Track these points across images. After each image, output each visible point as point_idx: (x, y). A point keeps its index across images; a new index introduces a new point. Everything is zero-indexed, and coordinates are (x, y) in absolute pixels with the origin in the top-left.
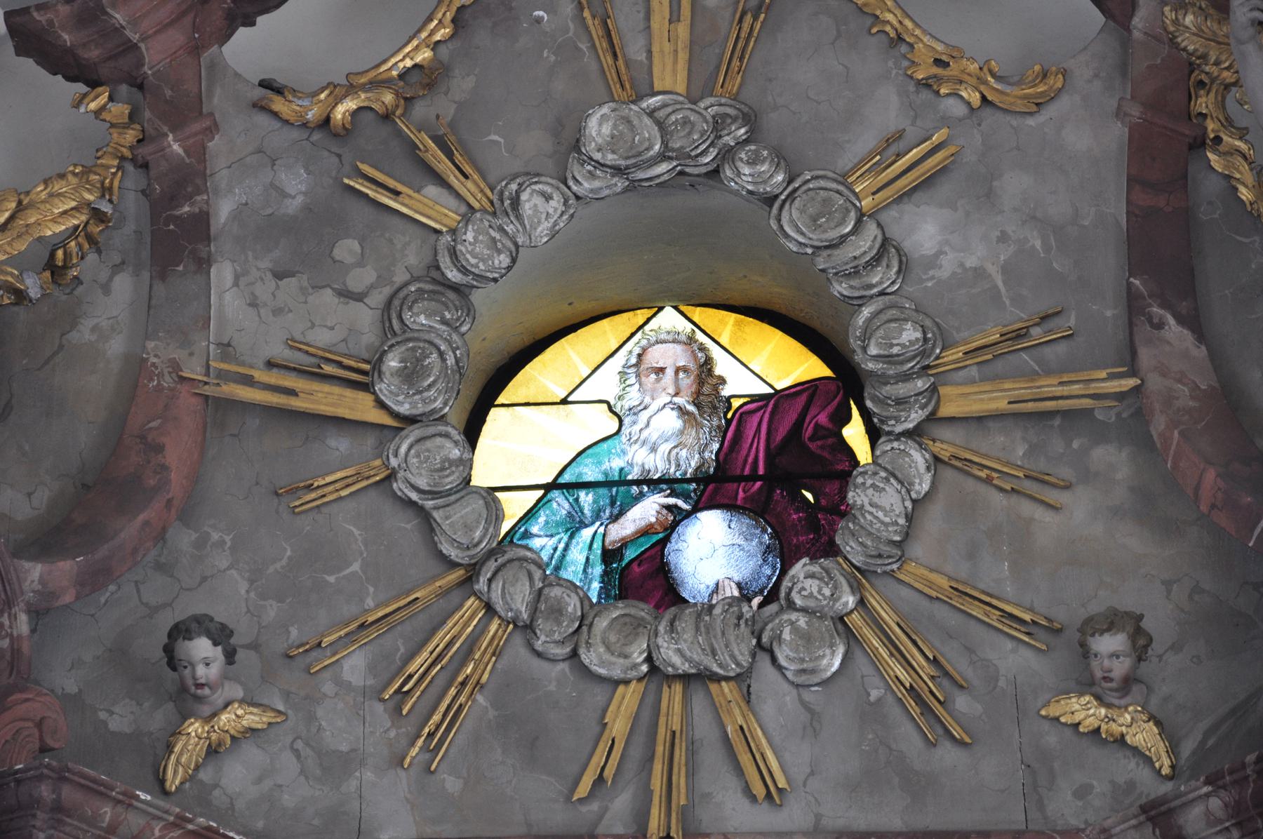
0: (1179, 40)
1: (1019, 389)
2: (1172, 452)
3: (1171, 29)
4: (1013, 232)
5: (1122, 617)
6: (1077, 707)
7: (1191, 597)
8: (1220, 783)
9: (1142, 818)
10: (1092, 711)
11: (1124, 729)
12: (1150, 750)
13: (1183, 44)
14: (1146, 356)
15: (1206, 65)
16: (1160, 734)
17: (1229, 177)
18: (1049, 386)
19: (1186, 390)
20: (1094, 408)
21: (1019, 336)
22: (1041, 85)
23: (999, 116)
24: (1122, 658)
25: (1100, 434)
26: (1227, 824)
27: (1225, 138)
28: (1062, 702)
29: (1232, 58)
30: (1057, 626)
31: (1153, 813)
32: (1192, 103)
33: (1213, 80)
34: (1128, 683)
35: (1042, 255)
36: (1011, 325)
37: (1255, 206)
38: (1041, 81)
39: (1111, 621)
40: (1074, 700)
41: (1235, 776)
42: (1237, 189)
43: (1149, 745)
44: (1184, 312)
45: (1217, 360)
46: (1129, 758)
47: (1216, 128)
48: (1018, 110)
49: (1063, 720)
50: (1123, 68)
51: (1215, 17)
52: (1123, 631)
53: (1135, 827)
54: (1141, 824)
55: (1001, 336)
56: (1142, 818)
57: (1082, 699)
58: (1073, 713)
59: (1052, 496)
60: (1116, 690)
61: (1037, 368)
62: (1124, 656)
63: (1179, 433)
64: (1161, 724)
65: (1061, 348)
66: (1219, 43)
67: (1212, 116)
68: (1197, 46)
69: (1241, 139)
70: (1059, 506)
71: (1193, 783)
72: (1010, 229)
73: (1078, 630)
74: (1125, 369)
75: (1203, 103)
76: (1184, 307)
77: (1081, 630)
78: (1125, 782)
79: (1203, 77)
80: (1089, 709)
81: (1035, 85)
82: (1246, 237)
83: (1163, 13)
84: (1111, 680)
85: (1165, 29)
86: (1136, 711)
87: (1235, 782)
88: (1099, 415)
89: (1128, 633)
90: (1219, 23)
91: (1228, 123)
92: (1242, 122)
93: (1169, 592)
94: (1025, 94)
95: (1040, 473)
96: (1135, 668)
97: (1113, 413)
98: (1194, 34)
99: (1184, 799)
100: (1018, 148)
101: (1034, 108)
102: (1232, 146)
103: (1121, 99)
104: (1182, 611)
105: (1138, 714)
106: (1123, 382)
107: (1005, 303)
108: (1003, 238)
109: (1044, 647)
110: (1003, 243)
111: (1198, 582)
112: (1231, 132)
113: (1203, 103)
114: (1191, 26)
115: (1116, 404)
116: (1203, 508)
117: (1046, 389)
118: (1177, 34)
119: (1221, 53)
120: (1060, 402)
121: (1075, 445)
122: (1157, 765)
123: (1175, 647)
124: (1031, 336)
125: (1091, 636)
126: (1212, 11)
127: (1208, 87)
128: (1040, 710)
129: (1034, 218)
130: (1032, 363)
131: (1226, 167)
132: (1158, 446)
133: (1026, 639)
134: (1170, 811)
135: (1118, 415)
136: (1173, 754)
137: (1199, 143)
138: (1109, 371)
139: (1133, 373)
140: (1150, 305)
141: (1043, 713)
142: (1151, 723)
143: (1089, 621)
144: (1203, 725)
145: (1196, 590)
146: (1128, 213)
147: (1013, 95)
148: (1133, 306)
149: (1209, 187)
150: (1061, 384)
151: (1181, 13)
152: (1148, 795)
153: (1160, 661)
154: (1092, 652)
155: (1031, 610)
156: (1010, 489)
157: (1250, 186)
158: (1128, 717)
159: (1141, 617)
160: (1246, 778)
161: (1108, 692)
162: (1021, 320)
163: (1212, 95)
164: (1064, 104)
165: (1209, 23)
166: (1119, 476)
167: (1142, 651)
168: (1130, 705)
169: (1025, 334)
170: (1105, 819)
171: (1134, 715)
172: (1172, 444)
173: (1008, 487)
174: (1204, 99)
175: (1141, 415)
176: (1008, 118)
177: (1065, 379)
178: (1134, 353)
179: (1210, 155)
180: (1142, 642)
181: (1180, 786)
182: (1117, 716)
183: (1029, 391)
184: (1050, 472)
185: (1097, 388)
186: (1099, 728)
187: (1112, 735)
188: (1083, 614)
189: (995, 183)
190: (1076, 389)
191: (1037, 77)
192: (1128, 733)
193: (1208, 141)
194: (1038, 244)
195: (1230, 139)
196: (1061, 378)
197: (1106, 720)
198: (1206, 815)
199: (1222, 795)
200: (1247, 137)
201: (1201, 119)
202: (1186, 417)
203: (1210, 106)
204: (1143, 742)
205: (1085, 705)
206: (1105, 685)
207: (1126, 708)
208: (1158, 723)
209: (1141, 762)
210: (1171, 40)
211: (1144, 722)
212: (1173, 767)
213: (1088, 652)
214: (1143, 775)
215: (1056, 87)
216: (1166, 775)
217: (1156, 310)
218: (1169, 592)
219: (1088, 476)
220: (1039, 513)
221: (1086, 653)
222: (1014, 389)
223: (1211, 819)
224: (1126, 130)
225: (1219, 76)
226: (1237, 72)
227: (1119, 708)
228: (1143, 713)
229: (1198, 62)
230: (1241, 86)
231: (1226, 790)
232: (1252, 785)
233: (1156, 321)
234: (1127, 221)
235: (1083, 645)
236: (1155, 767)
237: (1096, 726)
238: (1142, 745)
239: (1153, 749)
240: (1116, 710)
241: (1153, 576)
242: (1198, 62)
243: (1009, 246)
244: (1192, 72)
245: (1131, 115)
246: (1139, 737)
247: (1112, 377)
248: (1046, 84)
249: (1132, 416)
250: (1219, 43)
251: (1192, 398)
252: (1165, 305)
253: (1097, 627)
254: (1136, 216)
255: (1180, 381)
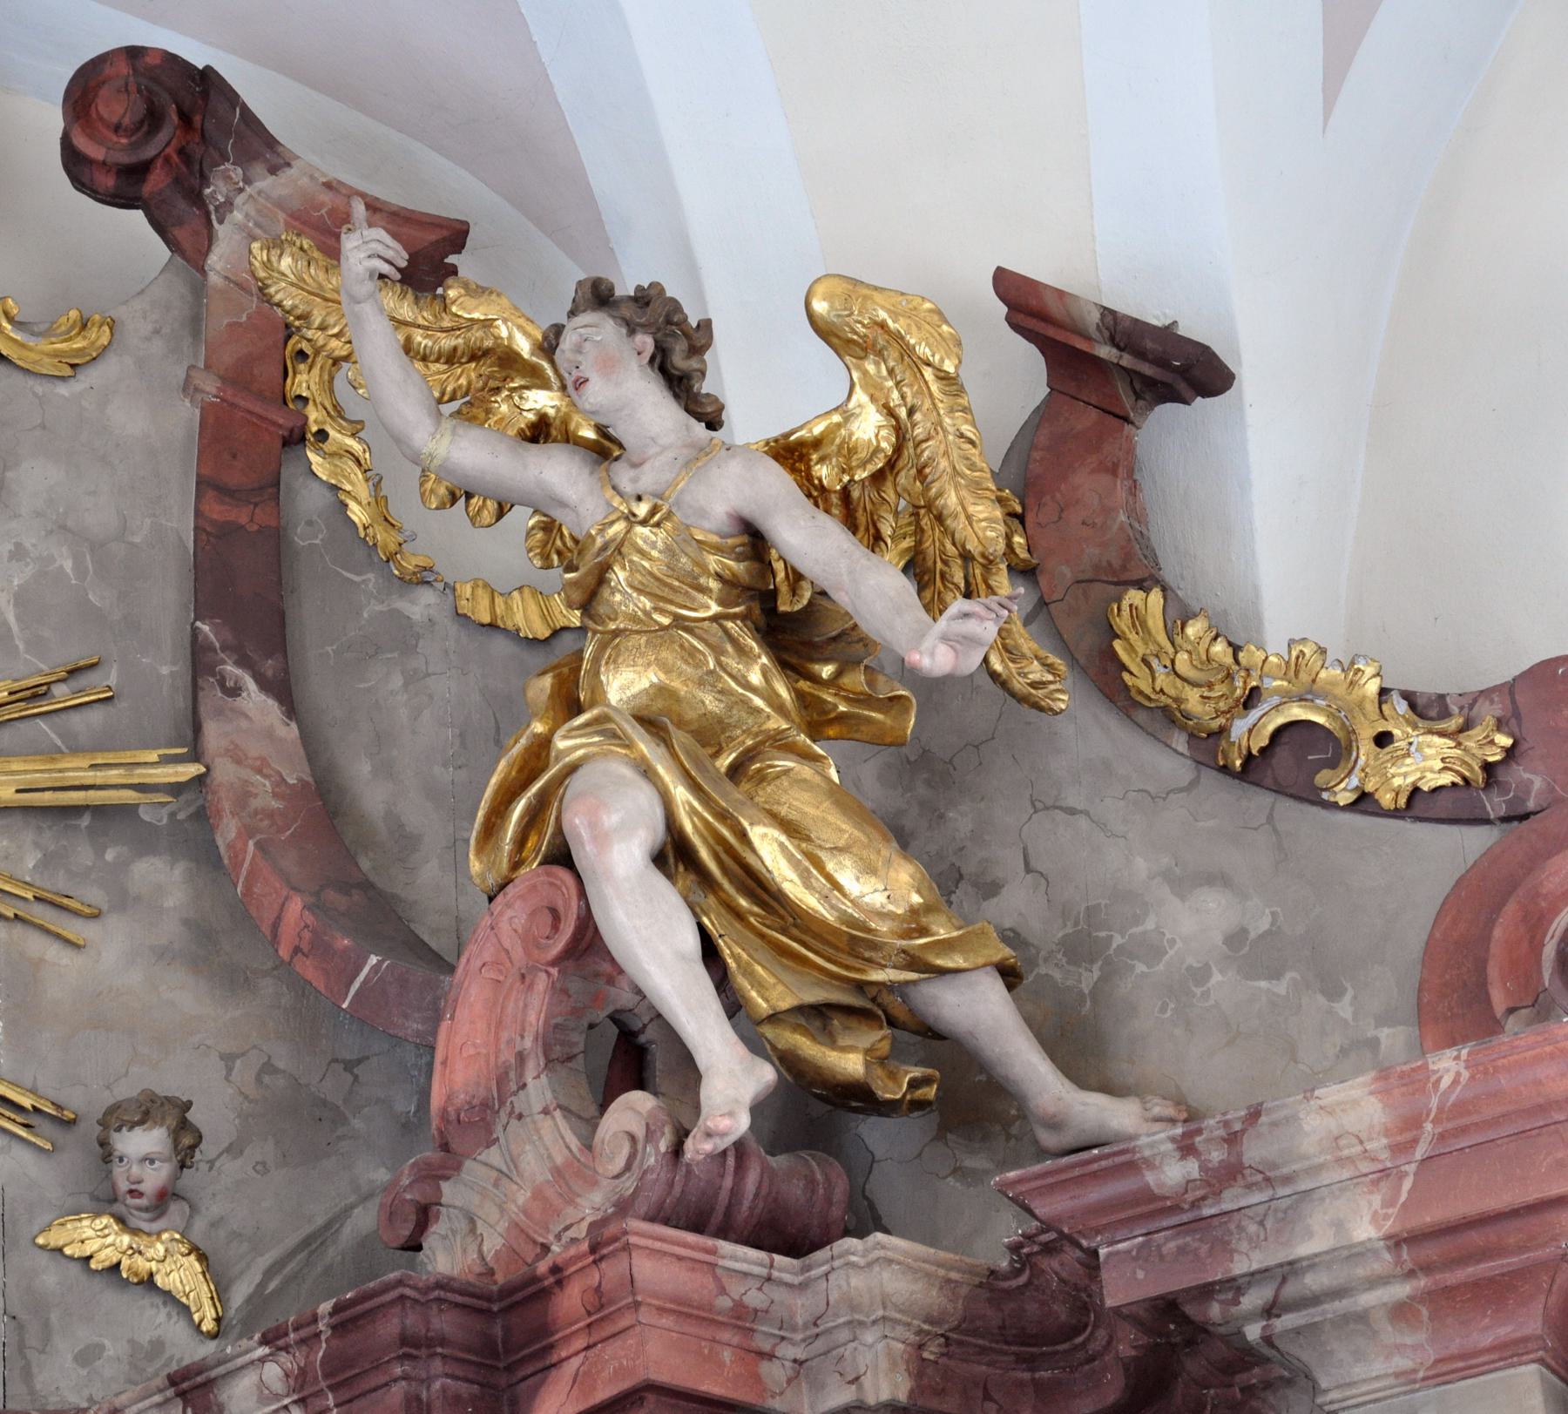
0: (272, 290)
1: (32, 771)
2: (244, 872)
3: (262, 274)
4: (34, 545)
5: (162, 1104)
6: (90, 1233)
7: (259, 1080)
8: (281, 1343)
9: (170, 1392)
10: (110, 1240)
11: (154, 1265)
12: (187, 1296)
13: (278, 298)
14: (214, 734)
15: (309, 328)
16: (203, 1273)
17: (335, 488)
18: (76, 769)
19: (267, 783)
20: (138, 805)
21: (35, 697)
22: (80, 338)
23: (18, 378)
24: (157, 1164)
25: (146, 841)
26: (286, 1401)
27: (332, 433)
28: (69, 1226)
29: (344, 321)
30: (69, 1115)
31: (185, 1385)
32: (289, 381)
33: (317, 352)
34: (164, 1199)
35: (74, 582)
36: (24, 678)
37: (370, 531)
38: (79, 333)
39: (146, 1110)
40: (86, 1223)
41: (303, 1333)
42: (347, 505)
43: (187, 1289)
44: (270, 673)
45: (311, 743)
46: (157, 1307)
47: (320, 418)
48: (45, 372)
49: (68, 1251)
50: (195, 323)
51: (321, 263)
52: (161, 1125)
53: (159, 1405)
54: (167, 1401)
55: (10, 694)
56: (170, 1392)
57: (98, 1221)
58: (83, 1242)
59: (73, 928)
60: (147, 1210)
61: (59, 743)
62: (162, 1161)
63: (257, 844)
64: (207, 1259)
65: (96, 716)
66: (326, 300)
67: (314, 401)
68: (297, 302)
69: (353, 435)
70: (81, 942)
71: (244, 1343)
72: (28, 543)
73: (99, 1123)
74: (185, 750)
75: (304, 382)
76: (269, 667)
77: (103, 1123)
78: (150, 1342)
79: (304, 346)
80: (106, 1236)
81: (70, 339)
82: (357, 574)
83: (250, 252)
84: (140, 1195)
85: (253, 274)
86: (173, 1240)
87: (302, 1342)
88: (145, 815)
89: (168, 1128)
90: (327, 271)
91: (338, 412)
92: (354, 412)
93: (229, 1070)
94: (55, 350)
95: (57, 894)
96: (175, 1177)
97: (165, 812)
98: (292, 284)
99: (230, 1366)
100: (43, 427)
101: (68, 371)
102: (341, 445)
103: (192, 367)
104: (246, 1097)
105: (174, 1243)
106: (181, 768)
107: (17, 647)
108: (19, 553)
109: (48, 1146)
110: (17, 561)
111: (270, 1057)
112: (340, 425)
113: (304, 382)
114: (288, 272)
115: (170, 799)
116: (284, 953)
117: (71, 774)
118: (269, 282)
119: (328, 314)
120: (91, 793)
121: (110, 855)
122: (196, 1317)
123: (234, 1150)
124: (54, 697)
125: (115, 1130)
126: (316, 254)
127: (310, 360)
128: (36, 1237)
129: (64, 527)
130: (53, 736)
131: (334, 474)
132: (226, 861)
133: (22, 1133)
134: (210, 1384)
135: (172, 815)
136: (220, 1301)
137: (296, 438)
138: (161, 752)
139: (195, 756)
140: (223, 662)
141: (40, 1241)
142: (192, 1257)
143: (113, 1110)
144: (264, 1261)
145: (268, 1068)
146: (196, 528)
147: (39, 351)
148: (200, 661)
149: (307, 502)
150: (93, 767)
151: (275, 253)
152: (181, 1359)
153: (211, 1169)
154: (117, 1153)
155: (33, 1091)
156: (12, 915)
157: (364, 502)
158: (160, 1248)
159: (188, 1105)
160: (318, 1335)
161: (135, 1212)
162: (40, 673)
163: (316, 371)
164: (110, 368)
165: (312, 271)
166: (169, 903)
167: (186, 1155)
168: (166, 1230)
169: (45, 694)
170: (117, 1395)
171: (169, 1245)
172: (244, 860)
173: (10, 914)
174: (305, 377)
175: (203, 817)
176: (31, 382)
177: (99, 761)
178: (197, 728)
179: (312, 456)
180: (187, 1141)
181: (226, 1346)
182: (146, 1246)
183: (46, 775)
184: (70, 894)
185: (144, 776)
186: (119, 1264)
187: (136, 1274)
188: (108, 1100)
189: (9, 474)
190: (114, 775)
191: (72, 327)
192: (158, 1271)
193: (309, 436)
194: (68, 565)
195: (339, 436)
196: (93, 759)
197: (130, 1252)
198: (258, 1388)
199: (282, 1360)
200: (361, 434)
201: (300, 404)
202: (266, 822)
203: (313, 386)
204: (179, 1285)
205: (101, 1230)
206: (130, 1201)
207: (159, 1234)
208: (202, 1258)
209: (174, 1313)
210: (261, 289)
211: (183, 1255)
212: (218, 1320)
213: (110, 1155)
214: (175, 1332)
215: (99, 343)
216: (208, 1332)
217: (230, 669)
218: (229, 1070)
219: (123, 901)
220: (53, 952)
221: (107, 1154)
222: (26, 772)
223: (264, 1394)
224: (198, 412)
225: (324, 345)
226: (350, 342)
227: (149, 1234)
228: (183, 1243)
229: (297, 323)
230: (355, 362)
231: (288, 1352)
232: (324, 1345)
233: (230, 684)
234: (195, 541)
235: (104, 1143)
236: (192, 1320)
237: (115, 1260)
238: (176, 1287)
239: (192, 1295)
240: (145, 1237)
241: (208, 1047)
242: (297, 323)
243: (27, 565)
244: (289, 337)
245: (203, 391)
246: (174, 1275)
247: (166, 760)
248: (84, 338)
249: (190, 817)
250: (326, 300)
251: (275, 795)
252: (244, 662)
253: (125, 1118)
254: (208, 534)
255: (259, 771)
